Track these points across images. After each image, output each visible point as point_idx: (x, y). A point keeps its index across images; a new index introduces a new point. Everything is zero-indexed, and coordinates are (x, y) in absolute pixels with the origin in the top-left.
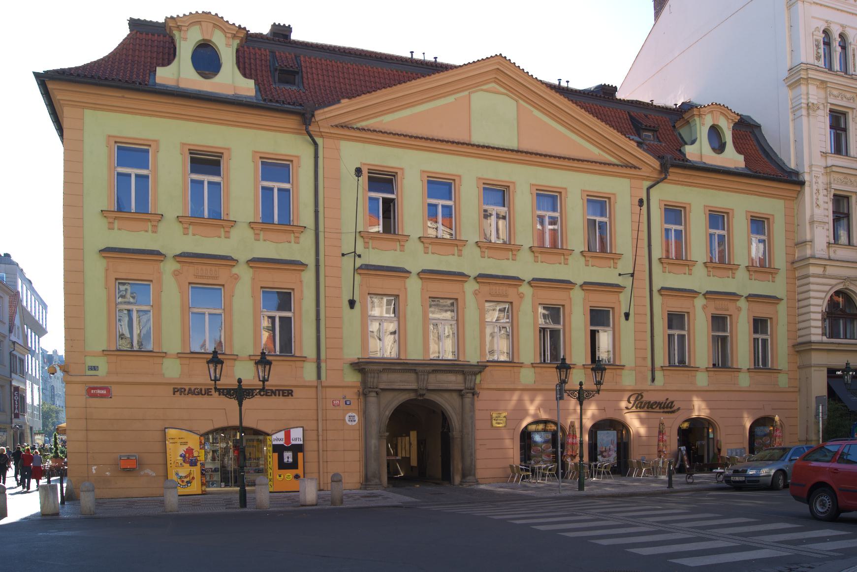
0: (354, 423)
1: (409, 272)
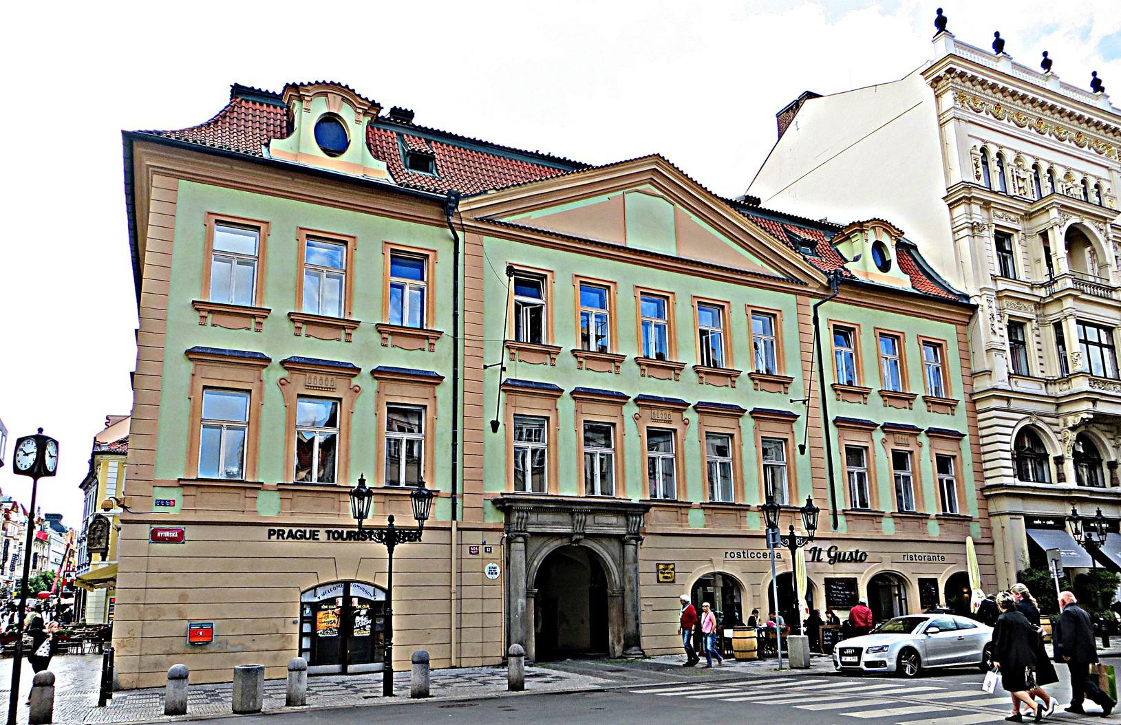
0: (495, 577)
1: (269, 360)
